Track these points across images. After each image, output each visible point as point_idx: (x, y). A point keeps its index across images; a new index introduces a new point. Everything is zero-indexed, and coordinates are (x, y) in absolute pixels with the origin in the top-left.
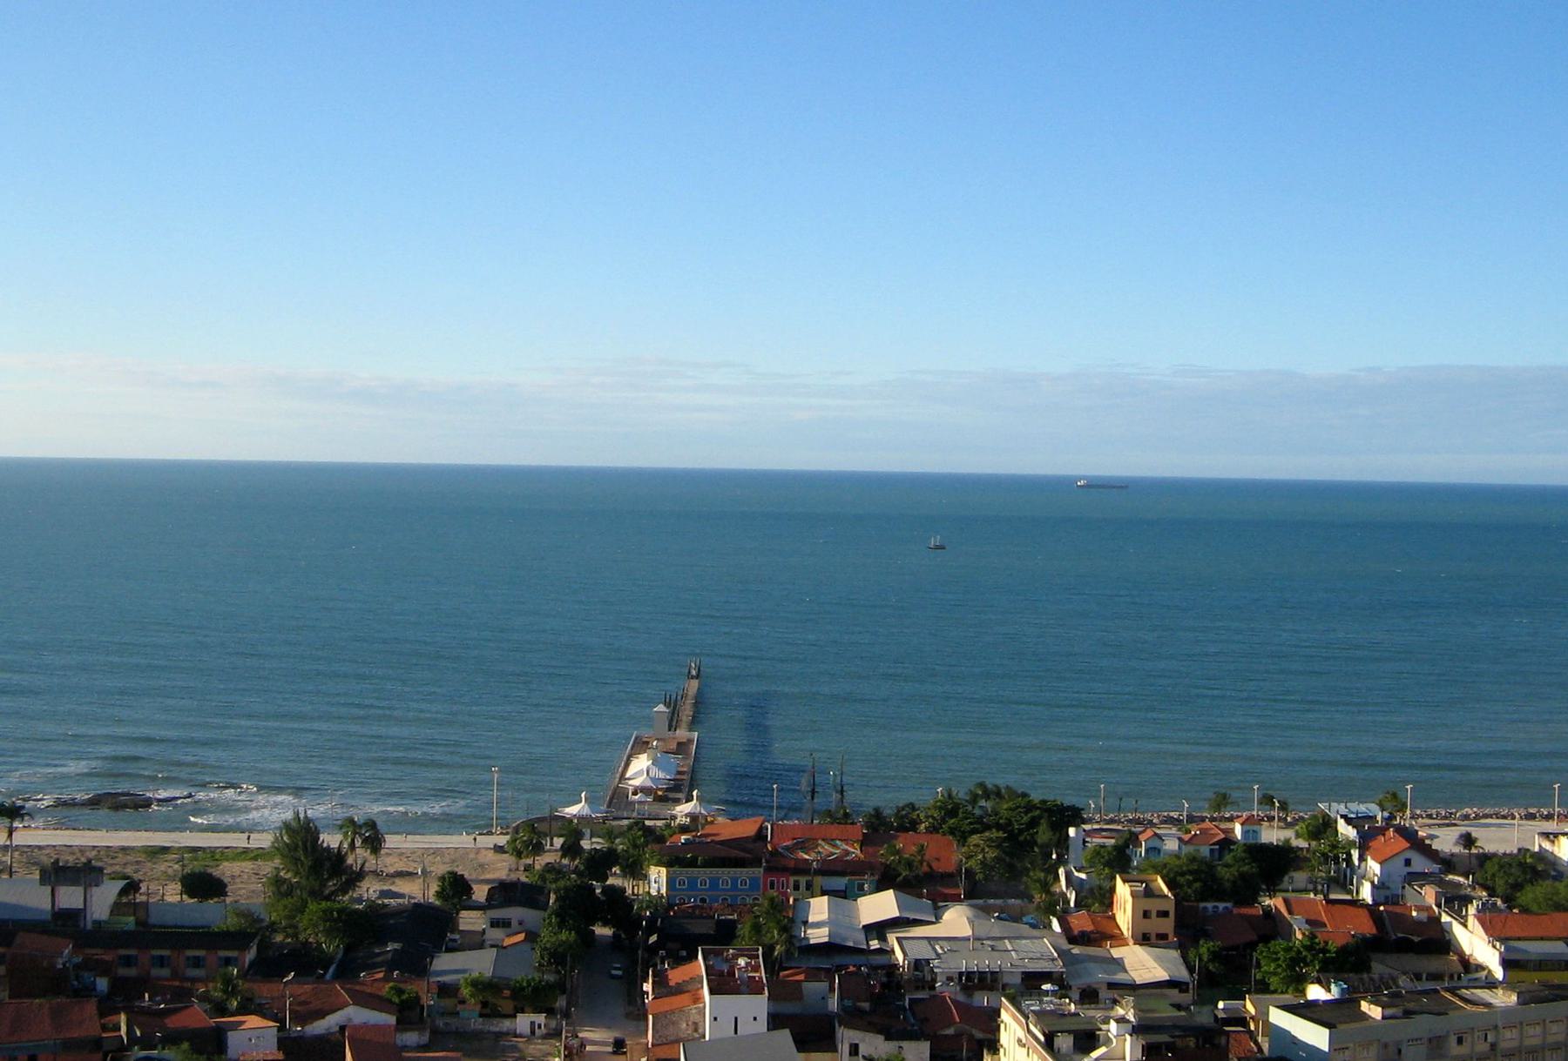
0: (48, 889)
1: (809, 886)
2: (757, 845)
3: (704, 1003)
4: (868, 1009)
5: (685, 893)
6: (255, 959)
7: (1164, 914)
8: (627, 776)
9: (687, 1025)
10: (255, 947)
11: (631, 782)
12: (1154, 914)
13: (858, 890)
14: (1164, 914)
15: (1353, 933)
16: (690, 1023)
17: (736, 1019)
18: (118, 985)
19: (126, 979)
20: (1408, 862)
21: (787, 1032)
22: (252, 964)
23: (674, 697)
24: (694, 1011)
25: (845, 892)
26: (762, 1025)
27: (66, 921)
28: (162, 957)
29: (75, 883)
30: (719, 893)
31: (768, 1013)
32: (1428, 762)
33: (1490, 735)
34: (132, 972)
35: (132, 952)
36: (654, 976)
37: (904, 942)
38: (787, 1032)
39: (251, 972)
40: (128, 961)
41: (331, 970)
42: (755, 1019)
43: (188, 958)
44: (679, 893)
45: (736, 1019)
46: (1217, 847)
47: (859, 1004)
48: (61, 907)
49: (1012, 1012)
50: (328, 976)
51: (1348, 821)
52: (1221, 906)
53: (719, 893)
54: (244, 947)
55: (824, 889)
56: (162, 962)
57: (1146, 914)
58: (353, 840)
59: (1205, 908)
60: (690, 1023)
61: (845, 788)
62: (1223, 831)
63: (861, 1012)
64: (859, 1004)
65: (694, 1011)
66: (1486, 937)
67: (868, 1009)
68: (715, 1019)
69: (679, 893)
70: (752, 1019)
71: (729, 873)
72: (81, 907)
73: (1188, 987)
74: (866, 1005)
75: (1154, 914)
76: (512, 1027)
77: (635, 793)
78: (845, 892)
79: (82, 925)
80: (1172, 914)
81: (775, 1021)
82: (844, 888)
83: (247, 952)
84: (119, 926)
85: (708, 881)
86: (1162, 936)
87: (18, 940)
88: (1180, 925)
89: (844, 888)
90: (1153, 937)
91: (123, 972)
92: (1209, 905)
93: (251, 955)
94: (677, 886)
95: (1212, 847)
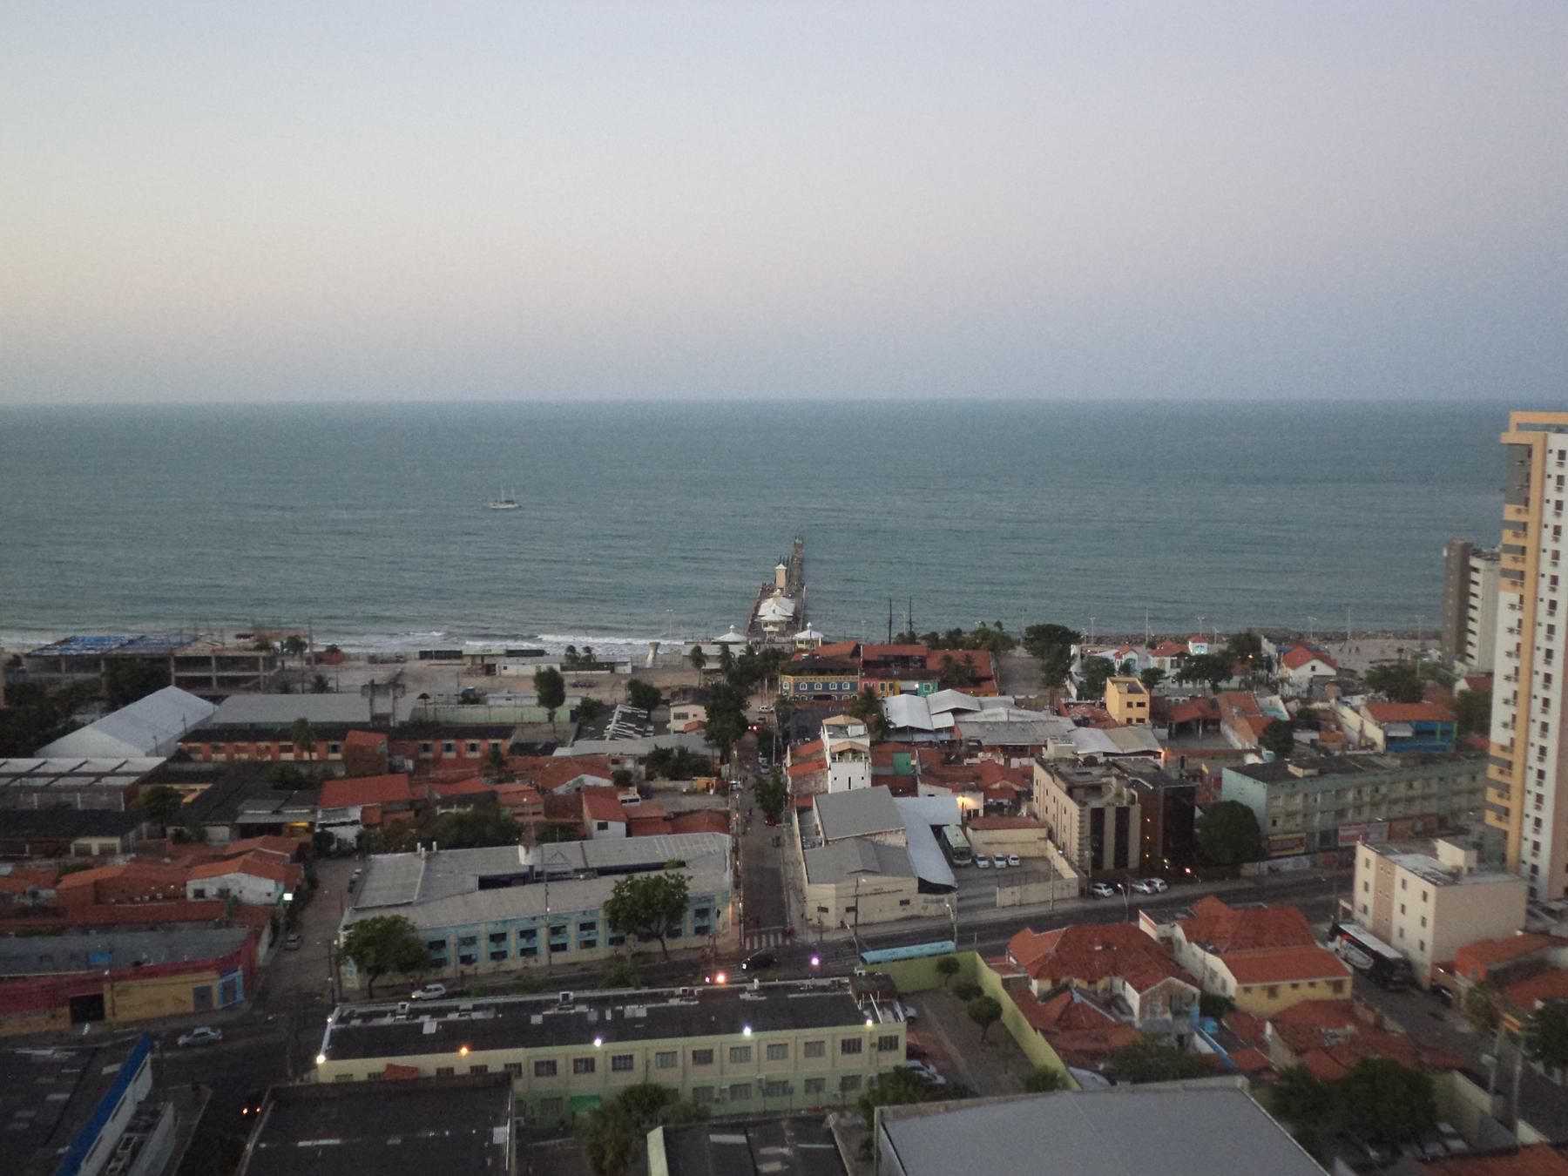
0: (367, 700)
1: (891, 687)
4: (438, 808)
7: (1141, 705)
8: (760, 614)
12: (1135, 705)
14: (1141, 705)
18: (420, 764)
20: (1313, 668)
21: (885, 786)
26: (868, 782)
27: (379, 723)
29: (386, 694)
34: (430, 755)
35: (452, 742)
38: (885, 786)
40: (426, 748)
50: (1348, 906)
51: (1271, 639)
56: (449, 748)
57: (1130, 705)
58: (450, 567)
66: (1373, 720)
67: (438, 808)
75: (1135, 705)
76: (70, 800)
77: (766, 625)
80: (1148, 705)
81: (876, 780)
88: (1153, 715)
91: (423, 755)
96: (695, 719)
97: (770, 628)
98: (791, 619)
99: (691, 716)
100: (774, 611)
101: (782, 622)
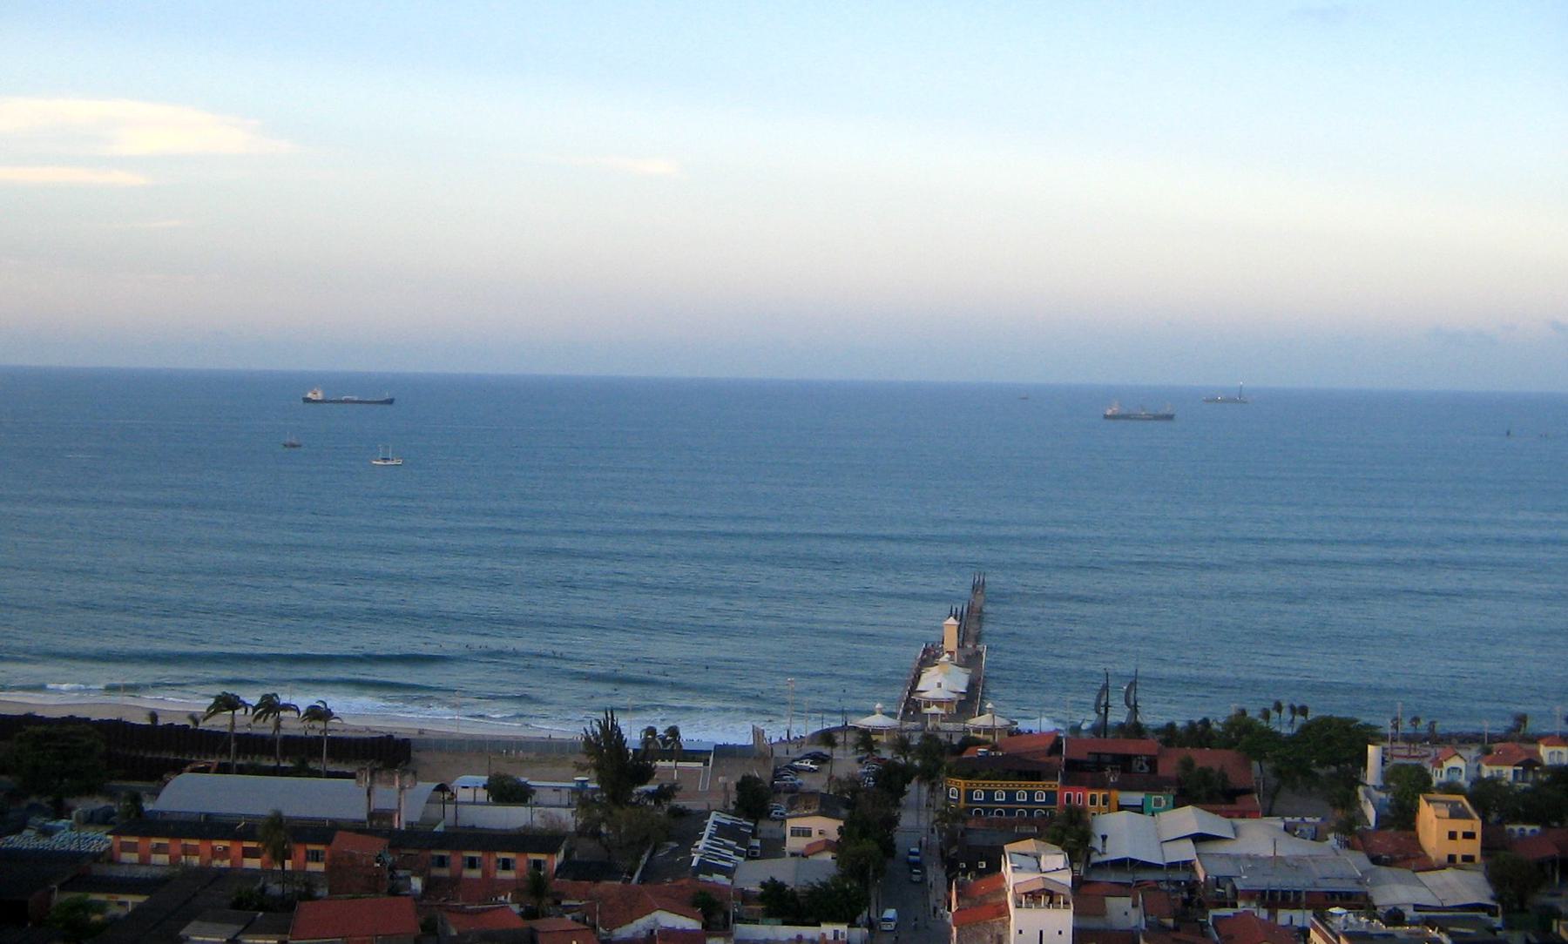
2: (1052, 758)
3: (1010, 916)
5: (1003, 806)
6: (563, 862)
8: (919, 688)
9: (992, 937)
10: (563, 852)
11: (923, 694)
12: (1460, 835)
13: (1091, 804)
14: (1469, 836)
15: (604, 829)
16: (994, 935)
17: (1041, 932)
19: (439, 880)
22: (560, 867)
23: (959, 610)
24: (998, 924)
25: (1142, 806)
28: (317, 852)
30: (1034, 806)
31: (1073, 928)
32: (791, 671)
33: (1484, 664)
34: (445, 872)
35: (477, 854)
36: (957, 888)
37: (1013, 855)
39: (559, 875)
40: (442, 862)
41: (637, 876)
42: (1060, 933)
43: (498, 861)
44: (997, 806)
45: (1041, 932)
46: (1521, 768)
47: (1162, 920)
48: (376, 807)
49: (1322, 931)
52: (1528, 828)
53: (1034, 806)
54: (553, 851)
55: (1121, 803)
56: (472, 863)
57: (1452, 836)
59: (1512, 830)
60: (994, 935)
61: (1138, 704)
62: (1528, 752)
63: (1164, 927)
64: (1162, 920)
65: (998, 924)
68: (1021, 932)
69: (997, 806)
70: (1063, 933)
71: (1026, 786)
72: (396, 807)
73: (1497, 911)
74: (1170, 922)
75: (1460, 835)
78: (1142, 806)
79: (396, 826)
82: (1140, 804)
83: (555, 856)
84: (231, 819)
85: (983, 794)
86: (1468, 859)
87: (337, 839)
88: (1487, 848)
89: (1140, 804)
90: (1459, 859)
91: (437, 872)
92: (1516, 828)
93: (558, 859)
94: (1017, 799)
95: (1516, 768)
96: (821, 838)
97: (934, 709)
98: (963, 698)
99: (815, 833)
100: (939, 685)
101: (950, 701)
